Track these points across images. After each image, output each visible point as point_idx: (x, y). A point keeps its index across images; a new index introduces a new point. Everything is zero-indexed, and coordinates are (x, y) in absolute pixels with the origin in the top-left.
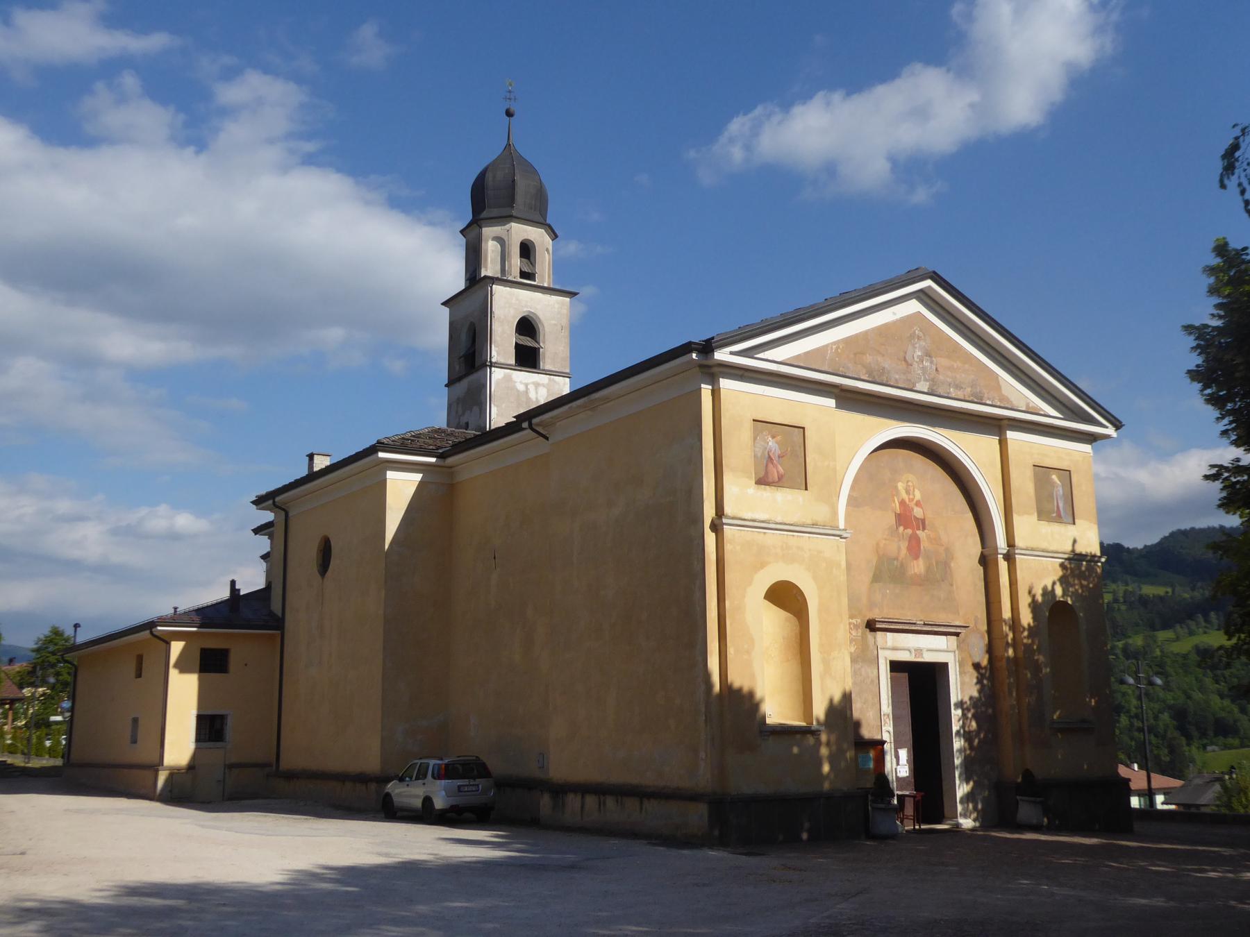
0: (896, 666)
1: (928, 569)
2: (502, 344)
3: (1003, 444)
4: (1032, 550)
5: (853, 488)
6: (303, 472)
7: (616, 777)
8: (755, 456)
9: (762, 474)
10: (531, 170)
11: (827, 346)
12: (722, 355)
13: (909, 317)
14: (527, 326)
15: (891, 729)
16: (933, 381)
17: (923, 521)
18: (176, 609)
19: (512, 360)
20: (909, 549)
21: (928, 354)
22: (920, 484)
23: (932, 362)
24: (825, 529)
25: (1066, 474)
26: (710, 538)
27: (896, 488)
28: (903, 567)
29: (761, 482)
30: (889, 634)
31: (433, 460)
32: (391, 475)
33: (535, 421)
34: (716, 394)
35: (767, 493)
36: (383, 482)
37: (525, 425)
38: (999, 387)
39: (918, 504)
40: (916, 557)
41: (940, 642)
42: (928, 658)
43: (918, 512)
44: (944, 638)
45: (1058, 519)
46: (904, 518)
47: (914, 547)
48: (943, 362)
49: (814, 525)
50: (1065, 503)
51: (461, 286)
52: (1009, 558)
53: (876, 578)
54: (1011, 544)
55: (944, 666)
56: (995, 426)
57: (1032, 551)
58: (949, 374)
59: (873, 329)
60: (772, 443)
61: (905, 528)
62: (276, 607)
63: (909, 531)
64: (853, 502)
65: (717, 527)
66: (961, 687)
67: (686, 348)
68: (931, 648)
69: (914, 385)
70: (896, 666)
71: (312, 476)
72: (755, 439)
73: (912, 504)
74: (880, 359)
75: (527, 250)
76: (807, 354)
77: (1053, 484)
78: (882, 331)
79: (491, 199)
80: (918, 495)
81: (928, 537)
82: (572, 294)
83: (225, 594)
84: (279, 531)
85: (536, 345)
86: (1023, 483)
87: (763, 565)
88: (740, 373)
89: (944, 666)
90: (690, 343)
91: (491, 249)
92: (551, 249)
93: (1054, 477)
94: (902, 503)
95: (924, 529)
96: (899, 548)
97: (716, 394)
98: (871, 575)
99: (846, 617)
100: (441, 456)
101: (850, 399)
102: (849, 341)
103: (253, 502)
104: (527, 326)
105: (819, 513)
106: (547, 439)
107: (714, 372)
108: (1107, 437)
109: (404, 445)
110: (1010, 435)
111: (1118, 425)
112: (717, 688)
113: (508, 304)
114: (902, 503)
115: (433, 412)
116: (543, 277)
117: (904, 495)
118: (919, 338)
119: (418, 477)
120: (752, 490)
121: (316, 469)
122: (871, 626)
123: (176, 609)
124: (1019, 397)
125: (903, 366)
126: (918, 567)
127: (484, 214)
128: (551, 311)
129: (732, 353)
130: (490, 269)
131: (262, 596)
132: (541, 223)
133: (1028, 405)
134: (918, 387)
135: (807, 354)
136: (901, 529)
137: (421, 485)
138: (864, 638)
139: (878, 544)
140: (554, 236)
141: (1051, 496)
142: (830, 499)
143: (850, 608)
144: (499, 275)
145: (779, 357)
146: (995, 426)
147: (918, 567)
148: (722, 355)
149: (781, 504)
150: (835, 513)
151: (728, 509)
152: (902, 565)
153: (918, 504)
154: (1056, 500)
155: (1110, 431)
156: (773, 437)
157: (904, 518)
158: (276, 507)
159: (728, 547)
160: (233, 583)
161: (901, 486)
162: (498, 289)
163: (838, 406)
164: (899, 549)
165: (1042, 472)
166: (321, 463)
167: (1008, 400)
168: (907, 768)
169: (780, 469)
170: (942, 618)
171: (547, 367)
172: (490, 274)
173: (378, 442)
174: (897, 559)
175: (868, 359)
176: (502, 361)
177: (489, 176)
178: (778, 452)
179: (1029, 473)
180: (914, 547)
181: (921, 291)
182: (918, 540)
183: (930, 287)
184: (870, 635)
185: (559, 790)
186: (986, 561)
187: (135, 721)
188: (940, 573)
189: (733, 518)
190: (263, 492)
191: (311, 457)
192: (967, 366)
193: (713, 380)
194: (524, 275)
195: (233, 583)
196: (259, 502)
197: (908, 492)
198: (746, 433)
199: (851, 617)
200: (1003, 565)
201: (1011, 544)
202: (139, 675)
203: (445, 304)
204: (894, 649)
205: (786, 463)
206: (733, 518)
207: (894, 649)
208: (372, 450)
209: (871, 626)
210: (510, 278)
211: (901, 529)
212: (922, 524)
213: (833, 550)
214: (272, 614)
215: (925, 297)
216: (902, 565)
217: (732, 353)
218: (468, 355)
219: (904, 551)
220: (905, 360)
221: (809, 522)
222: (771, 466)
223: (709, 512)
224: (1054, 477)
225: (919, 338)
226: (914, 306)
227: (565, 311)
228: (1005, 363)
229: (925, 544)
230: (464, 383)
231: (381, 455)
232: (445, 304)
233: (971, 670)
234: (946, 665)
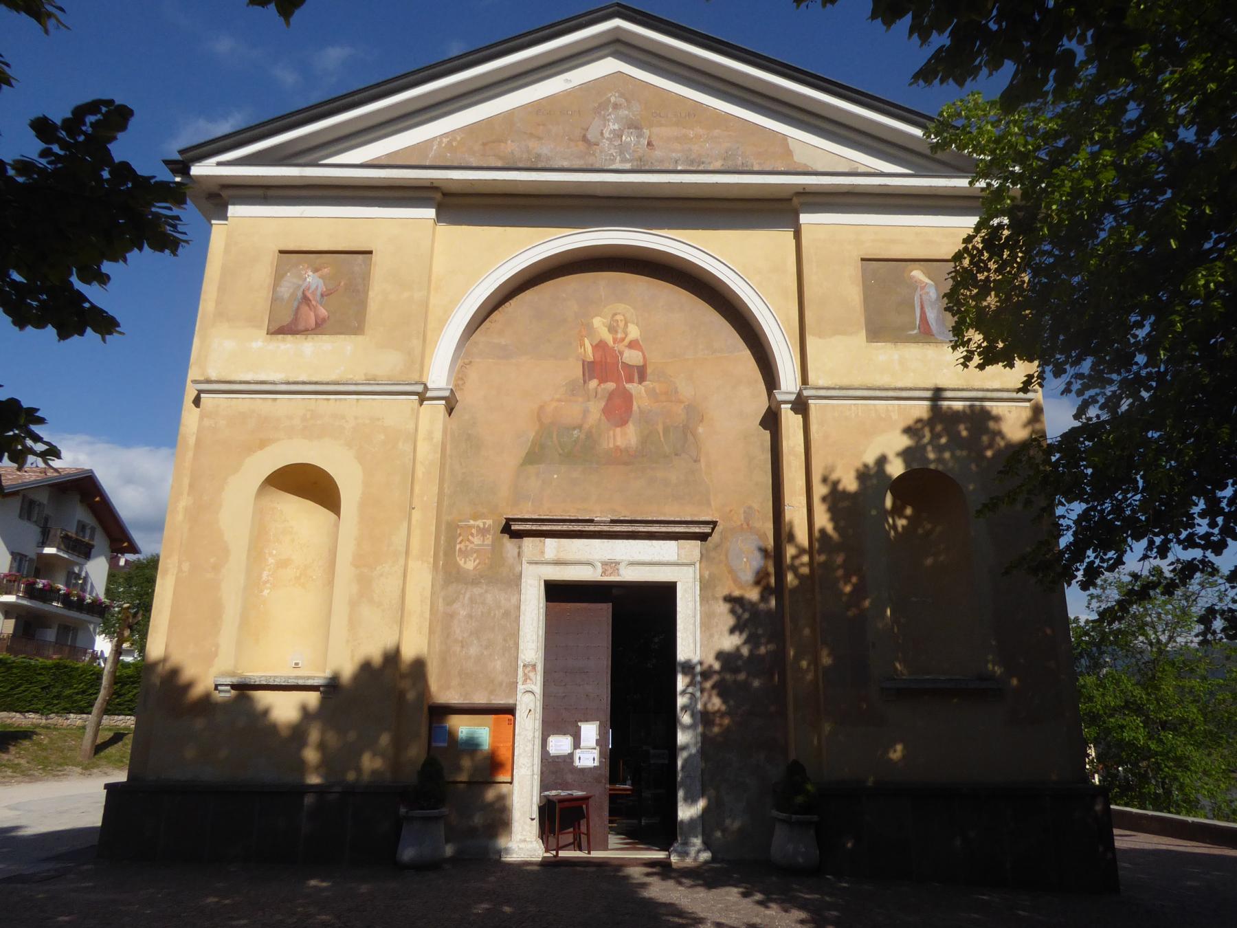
0: (556, 592)
1: (645, 440)
20: (607, 411)
21: (634, 126)
23: (639, 136)
28: (591, 439)
30: (548, 541)
35: (287, 345)
39: (633, 345)
40: (623, 423)
41: (667, 550)
43: (632, 357)
44: (673, 544)
47: (619, 407)
53: (534, 456)
56: (775, 209)
61: (602, 381)
63: (611, 386)
66: (699, 636)
68: (635, 561)
70: (556, 592)
73: (621, 347)
78: (537, 108)
80: (634, 332)
81: (652, 394)
87: (263, 444)
88: (260, 192)
98: (523, 454)
101: (460, 205)
102: (471, 129)
105: (387, 364)
109: (644, 357)
112: (802, 537)
114: (600, 346)
117: (608, 338)
118: (616, 106)
120: (259, 342)
122: (511, 530)
126: (627, 436)
138: (496, 549)
139: (541, 408)
147: (627, 436)
153: (633, 345)
156: (316, 270)
157: (603, 366)
161: (597, 322)
163: (440, 218)
164: (586, 412)
168: (596, 753)
174: (580, 427)
178: (322, 288)
180: (619, 407)
182: (628, 398)
184: (509, 545)
192: (716, 132)
197: (612, 329)
204: (558, 563)
207: (558, 563)
209: (511, 530)
211: (593, 384)
217: (219, 164)
220: (584, 139)
222: (305, 308)
228: (759, 100)
233: (724, 608)
234: (667, 592)
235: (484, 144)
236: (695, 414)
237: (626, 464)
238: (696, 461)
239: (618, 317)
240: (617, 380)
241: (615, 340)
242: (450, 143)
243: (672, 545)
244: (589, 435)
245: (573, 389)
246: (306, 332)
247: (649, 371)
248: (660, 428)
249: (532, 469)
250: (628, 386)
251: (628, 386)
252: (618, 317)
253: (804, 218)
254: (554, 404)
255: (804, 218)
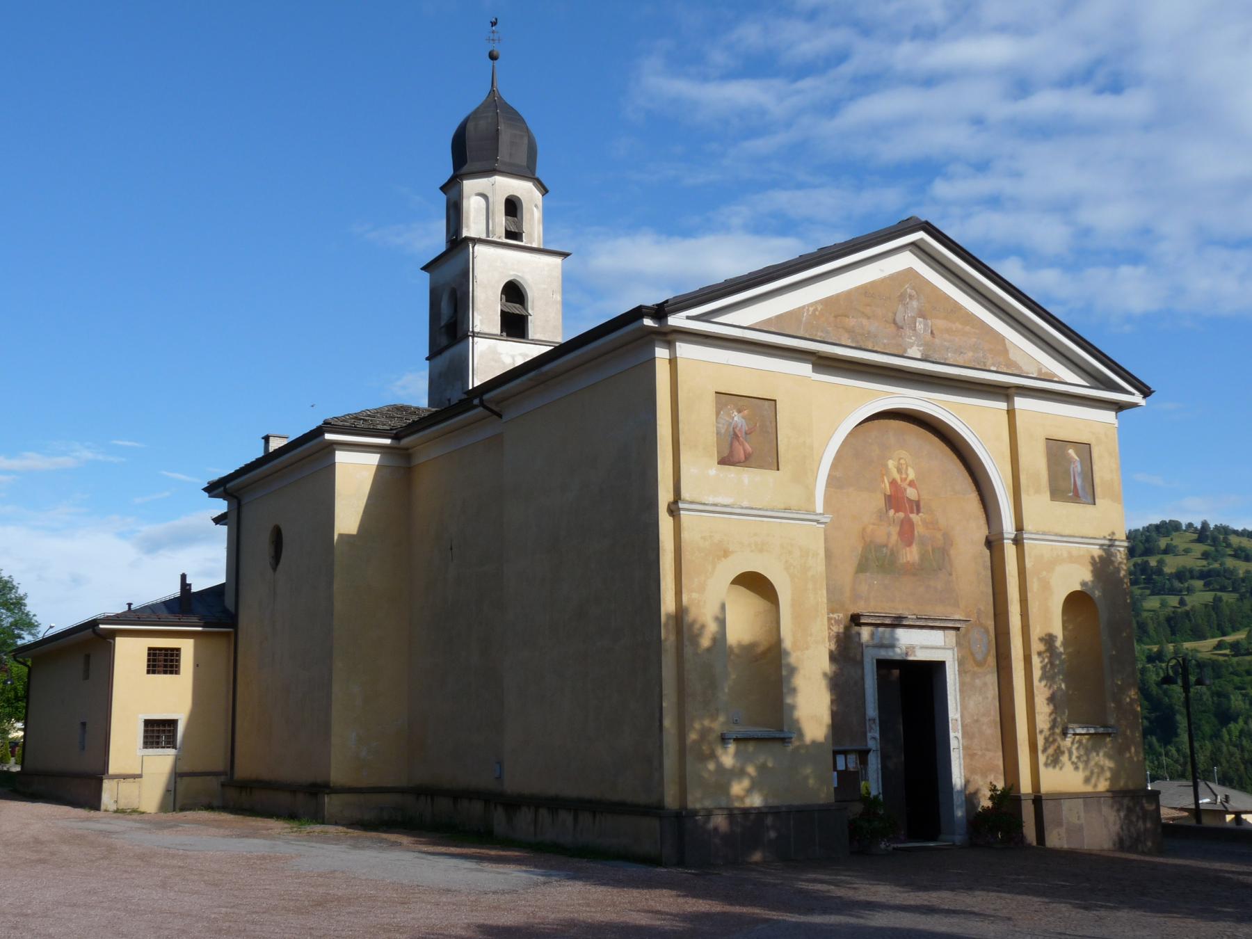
1: (923, 556)
2: (485, 311)
3: (1011, 413)
4: (1044, 534)
5: (834, 466)
6: (260, 454)
7: (570, 790)
8: (718, 433)
9: (726, 453)
10: (515, 118)
11: (803, 307)
12: (676, 320)
13: (899, 274)
14: (513, 292)
15: (877, 735)
16: (927, 345)
17: (918, 504)
18: (130, 605)
19: (497, 329)
20: (901, 534)
22: (913, 460)
24: (804, 514)
25: (1085, 449)
26: (665, 524)
27: (886, 466)
28: (893, 554)
29: (724, 461)
31: (388, 441)
32: (341, 457)
33: (486, 397)
34: (673, 362)
35: (732, 472)
36: (332, 466)
37: (476, 402)
38: (1006, 351)
39: (912, 484)
40: (910, 544)
42: (921, 656)
43: (911, 493)
45: (1076, 497)
46: (895, 500)
48: (941, 323)
49: (786, 509)
50: (1083, 480)
51: (442, 248)
52: (1018, 541)
53: (862, 568)
54: (1019, 528)
55: (940, 666)
56: (1003, 392)
57: (1044, 535)
58: (946, 336)
59: (857, 289)
60: (737, 418)
61: (897, 511)
62: (229, 602)
63: (901, 515)
64: (833, 481)
65: (674, 510)
67: (639, 313)
69: (905, 351)
71: (269, 457)
72: (718, 414)
73: (904, 485)
74: (865, 321)
75: (513, 207)
76: (779, 318)
77: (1070, 460)
79: (472, 151)
80: (912, 475)
81: (924, 521)
82: (565, 255)
83: (174, 590)
84: (233, 518)
85: (524, 313)
86: (1035, 461)
89: (940, 666)
90: (640, 308)
91: (473, 207)
92: (540, 204)
93: (1071, 452)
94: (893, 483)
95: (918, 511)
96: (889, 534)
97: (673, 362)
99: (824, 611)
100: (396, 437)
103: (205, 490)
104: (513, 292)
106: (500, 416)
107: (670, 337)
108: (1134, 405)
110: (1020, 403)
111: (1146, 392)
113: (490, 269)
114: (893, 483)
115: (413, 389)
116: (531, 235)
117: (897, 476)
119: (374, 459)
120: (714, 470)
121: (271, 450)
123: (130, 605)
124: (1031, 358)
125: (891, 329)
127: (465, 169)
128: (540, 274)
129: (688, 318)
130: (473, 226)
131: (215, 593)
132: (526, 172)
133: (1040, 370)
134: (910, 353)
135: (779, 317)
136: (892, 512)
137: (380, 467)
139: (864, 529)
140: (544, 191)
141: (1067, 472)
142: (804, 476)
143: (829, 600)
144: (483, 236)
145: (747, 318)
146: (1003, 392)
147: (911, 555)
148: (676, 320)
149: (746, 484)
150: (811, 497)
151: (685, 494)
152: (892, 553)
153: (912, 484)
154: (1071, 475)
155: (1137, 398)
156: (739, 411)
157: (895, 500)
158: (225, 495)
159: (685, 535)
160: (184, 577)
162: (479, 250)
164: (889, 535)
165: (1056, 448)
166: (275, 444)
167: (1019, 368)
169: (747, 446)
170: (938, 611)
171: (537, 337)
172: (473, 234)
173: (326, 423)
174: (886, 546)
175: (851, 322)
176: (486, 331)
177: (470, 126)
178: (745, 428)
179: (1041, 448)
181: (913, 244)
183: (922, 240)
185: (513, 804)
186: (993, 544)
187: (84, 724)
188: (937, 560)
189: (692, 503)
190: (215, 477)
191: (267, 439)
193: (670, 345)
194: (510, 234)
195: (184, 577)
196: (213, 489)
197: (899, 471)
198: (707, 408)
199: (831, 611)
200: (1010, 551)
201: (1019, 528)
202: (86, 677)
203: (425, 268)
205: (751, 437)
206: (692, 503)
208: (318, 432)
210: (495, 239)
211: (892, 512)
212: (916, 506)
213: (811, 538)
214: (225, 611)
215: (916, 247)
216: (892, 553)
217: (688, 318)
218: (449, 328)
219: (894, 537)
220: (894, 322)
221: (782, 506)
223: (665, 496)
224: (1071, 452)
225: (911, 297)
226: (908, 260)
227: (558, 273)
229: (919, 530)
230: (447, 355)
231: (328, 436)
232: (425, 268)
235: (836, 317)
236: (948, 540)
237: (915, 575)
238: (950, 574)
239: (902, 461)
240: (905, 512)
241: (902, 480)
242: (815, 310)
243: (940, 633)
244: (892, 551)
245: (881, 516)
246: (733, 464)
247: (922, 504)
248: (930, 549)
249: (861, 576)
250: (912, 516)
251: (912, 516)
252: (902, 461)
253: (465, 233)
254: (871, 527)
255: (465, 233)
